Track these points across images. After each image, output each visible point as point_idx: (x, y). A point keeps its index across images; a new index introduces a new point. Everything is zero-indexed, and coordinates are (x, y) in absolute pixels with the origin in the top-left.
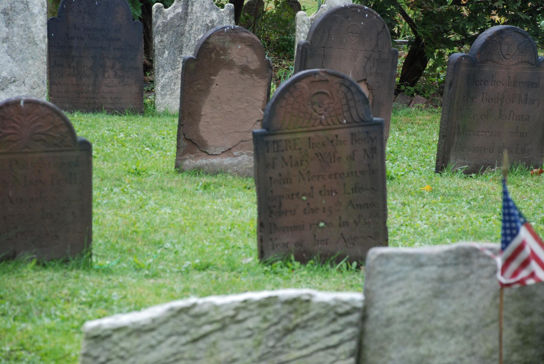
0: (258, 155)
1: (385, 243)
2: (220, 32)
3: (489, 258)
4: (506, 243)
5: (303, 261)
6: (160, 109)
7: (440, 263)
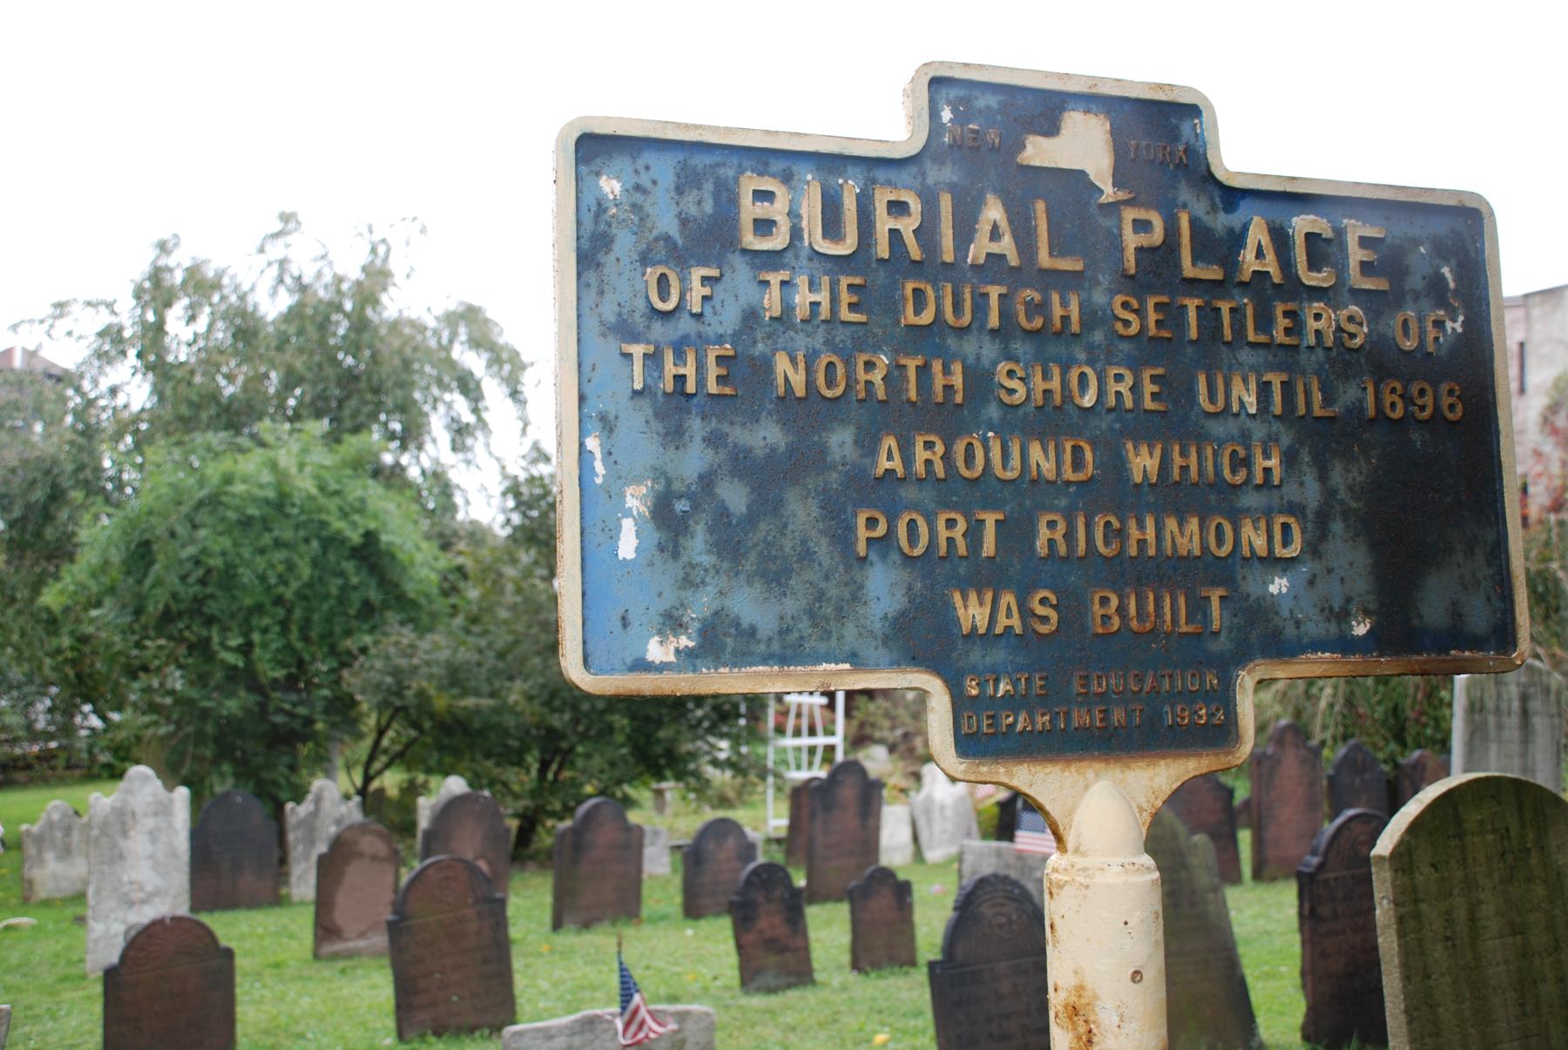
0: (393, 941)
1: (514, 1023)
2: (351, 828)
3: (610, 1022)
4: (624, 1008)
5: (438, 1034)
6: (296, 898)
7: (568, 1032)
